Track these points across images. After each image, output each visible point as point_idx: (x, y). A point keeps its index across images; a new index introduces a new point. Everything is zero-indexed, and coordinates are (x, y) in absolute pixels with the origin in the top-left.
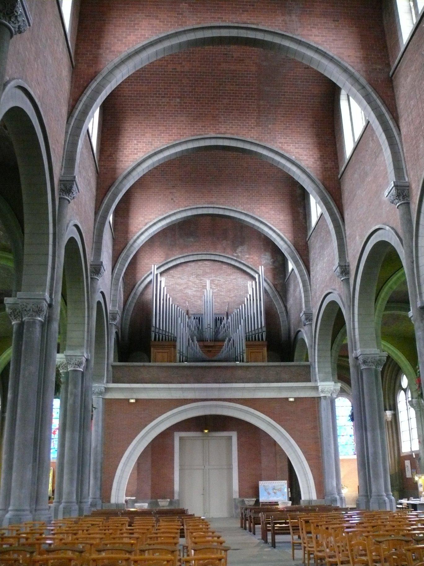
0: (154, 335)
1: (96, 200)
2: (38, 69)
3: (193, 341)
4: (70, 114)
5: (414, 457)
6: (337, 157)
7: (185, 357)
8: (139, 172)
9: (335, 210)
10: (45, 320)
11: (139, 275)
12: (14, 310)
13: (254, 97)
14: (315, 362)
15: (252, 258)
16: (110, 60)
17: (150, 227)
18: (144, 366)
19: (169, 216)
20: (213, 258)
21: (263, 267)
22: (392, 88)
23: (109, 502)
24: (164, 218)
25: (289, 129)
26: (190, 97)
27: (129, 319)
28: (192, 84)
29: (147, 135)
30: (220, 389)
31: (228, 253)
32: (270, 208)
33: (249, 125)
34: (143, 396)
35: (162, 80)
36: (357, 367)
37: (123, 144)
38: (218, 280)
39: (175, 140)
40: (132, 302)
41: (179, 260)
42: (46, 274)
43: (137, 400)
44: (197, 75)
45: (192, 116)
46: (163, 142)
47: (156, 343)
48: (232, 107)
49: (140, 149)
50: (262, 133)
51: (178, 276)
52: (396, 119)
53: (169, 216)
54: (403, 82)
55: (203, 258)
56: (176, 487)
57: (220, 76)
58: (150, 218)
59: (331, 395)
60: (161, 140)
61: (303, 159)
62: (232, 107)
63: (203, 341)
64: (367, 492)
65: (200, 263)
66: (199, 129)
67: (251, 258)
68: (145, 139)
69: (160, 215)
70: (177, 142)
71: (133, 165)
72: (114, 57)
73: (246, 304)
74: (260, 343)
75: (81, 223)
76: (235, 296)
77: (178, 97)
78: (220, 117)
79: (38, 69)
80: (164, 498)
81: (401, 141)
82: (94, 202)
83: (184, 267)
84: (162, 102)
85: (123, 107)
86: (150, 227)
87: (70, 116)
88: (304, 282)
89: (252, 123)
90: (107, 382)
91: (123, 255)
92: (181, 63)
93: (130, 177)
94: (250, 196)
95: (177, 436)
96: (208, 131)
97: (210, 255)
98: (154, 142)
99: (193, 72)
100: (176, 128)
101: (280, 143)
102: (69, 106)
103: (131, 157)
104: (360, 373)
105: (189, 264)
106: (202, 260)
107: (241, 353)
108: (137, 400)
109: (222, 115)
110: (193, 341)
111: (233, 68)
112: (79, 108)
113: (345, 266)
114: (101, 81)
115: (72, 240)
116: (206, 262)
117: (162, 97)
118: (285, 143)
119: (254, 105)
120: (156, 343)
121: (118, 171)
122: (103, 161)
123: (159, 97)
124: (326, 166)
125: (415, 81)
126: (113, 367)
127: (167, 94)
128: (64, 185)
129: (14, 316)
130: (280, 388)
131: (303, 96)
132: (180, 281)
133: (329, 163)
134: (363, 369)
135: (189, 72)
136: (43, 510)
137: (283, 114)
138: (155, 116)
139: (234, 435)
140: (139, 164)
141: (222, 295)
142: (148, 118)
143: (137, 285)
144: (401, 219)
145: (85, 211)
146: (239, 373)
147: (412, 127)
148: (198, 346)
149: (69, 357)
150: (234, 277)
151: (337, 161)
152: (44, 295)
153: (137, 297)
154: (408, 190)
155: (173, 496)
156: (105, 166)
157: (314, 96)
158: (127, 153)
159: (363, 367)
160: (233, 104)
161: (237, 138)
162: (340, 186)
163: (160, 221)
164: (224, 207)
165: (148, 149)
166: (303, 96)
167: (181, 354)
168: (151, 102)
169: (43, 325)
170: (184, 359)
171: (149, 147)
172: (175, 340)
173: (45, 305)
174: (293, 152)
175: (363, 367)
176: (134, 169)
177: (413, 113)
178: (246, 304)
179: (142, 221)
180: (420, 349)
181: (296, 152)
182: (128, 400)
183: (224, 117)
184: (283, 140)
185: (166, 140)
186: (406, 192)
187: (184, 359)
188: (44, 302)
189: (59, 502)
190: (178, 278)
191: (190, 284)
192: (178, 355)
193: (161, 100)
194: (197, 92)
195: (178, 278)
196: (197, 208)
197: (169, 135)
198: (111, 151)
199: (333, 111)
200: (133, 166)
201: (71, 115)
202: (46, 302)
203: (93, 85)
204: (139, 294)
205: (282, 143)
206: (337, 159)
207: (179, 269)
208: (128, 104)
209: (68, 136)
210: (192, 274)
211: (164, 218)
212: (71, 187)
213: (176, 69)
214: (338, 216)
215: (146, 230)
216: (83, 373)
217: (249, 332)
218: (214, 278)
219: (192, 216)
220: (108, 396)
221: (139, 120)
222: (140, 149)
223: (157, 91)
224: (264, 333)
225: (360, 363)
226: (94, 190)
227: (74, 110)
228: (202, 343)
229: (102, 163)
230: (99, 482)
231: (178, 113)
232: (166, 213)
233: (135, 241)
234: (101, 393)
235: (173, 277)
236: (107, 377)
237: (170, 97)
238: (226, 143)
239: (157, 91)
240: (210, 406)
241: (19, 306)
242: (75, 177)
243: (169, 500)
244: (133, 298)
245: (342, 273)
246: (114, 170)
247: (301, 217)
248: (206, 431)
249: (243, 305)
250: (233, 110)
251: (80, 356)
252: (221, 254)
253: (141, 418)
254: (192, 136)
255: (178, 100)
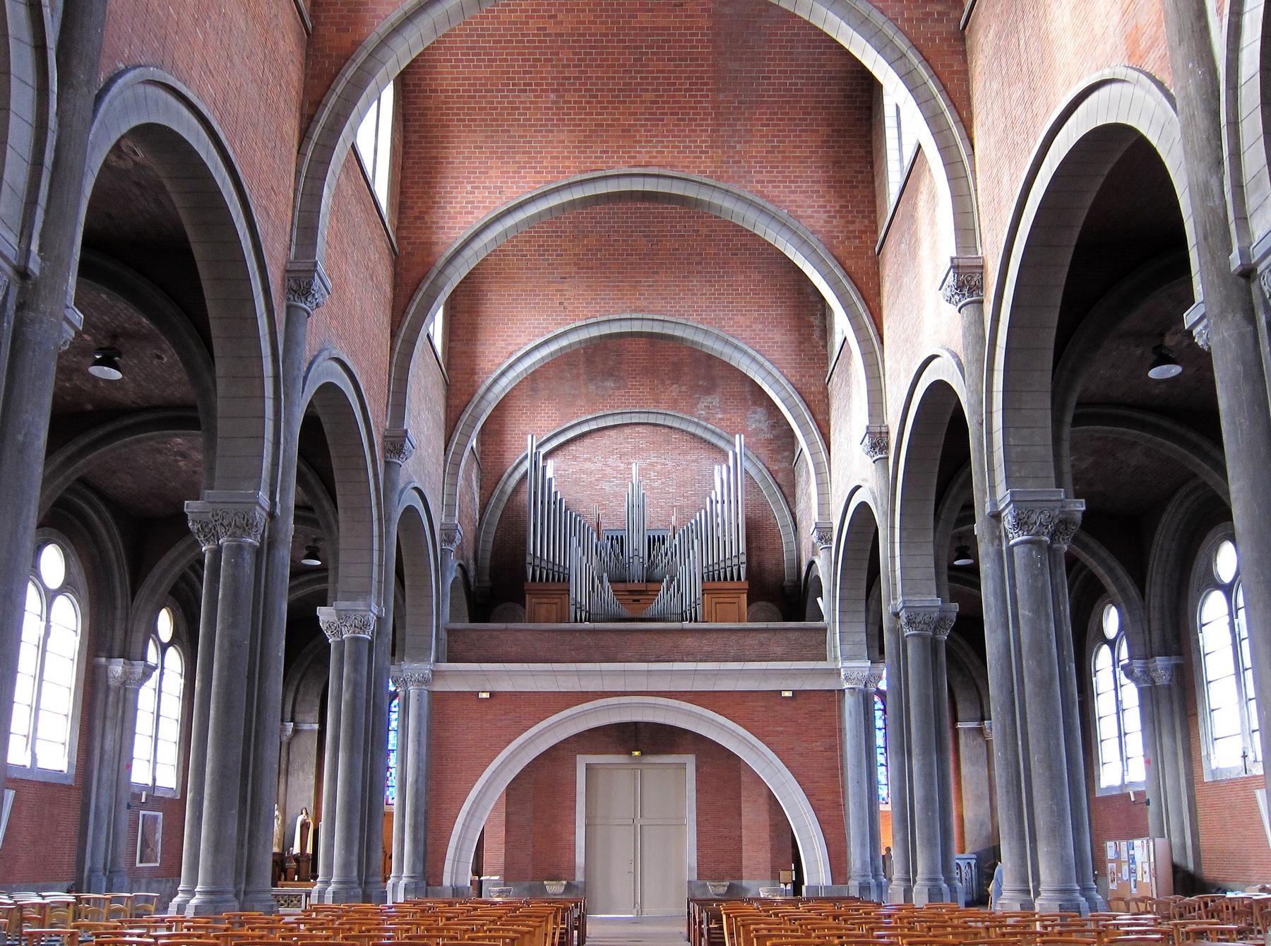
0: (531, 569)
1: (393, 309)
2: (205, 45)
3: (601, 582)
4: (304, 135)
5: (1133, 799)
6: (875, 207)
7: (586, 612)
8: (476, 249)
9: (866, 319)
10: (262, 543)
11: (508, 456)
12: (204, 525)
13: (706, 84)
14: (834, 622)
15: (730, 419)
16: (383, 16)
17: (519, 359)
18: (506, 630)
19: (556, 337)
20: (652, 419)
21: (742, 436)
22: (964, 53)
23: (441, 884)
24: (546, 343)
25: (778, 152)
26: (575, 90)
27: (491, 540)
28: (579, 60)
29: (492, 173)
30: (649, 673)
31: (681, 410)
32: (755, 318)
33: (695, 147)
34: (505, 686)
35: (519, 54)
36: (897, 632)
37: (445, 193)
38: (663, 464)
39: (548, 182)
40: (496, 507)
41: (578, 427)
42: (261, 456)
43: (492, 694)
44: (590, 41)
45: (580, 131)
46: (523, 187)
47: (537, 585)
48: (664, 108)
49: (479, 202)
50: (722, 162)
51: (585, 456)
52: (967, 126)
53: (556, 337)
54: (982, 40)
55: (634, 421)
56: (580, 859)
57: (635, 41)
58: (518, 342)
59: (865, 686)
60: (519, 182)
61: (804, 214)
62: (664, 108)
63: (625, 581)
64: (907, 872)
65: (627, 431)
66: (596, 157)
67: (727, 420)
68: (487, 181)
69: (537, 336)
70: (552, 186)
71: (465, 234)
72: (391, 8)
73: (708, 509)
74: (735, 585)
75: (353, 354)
76: (694, 495)
77: (553, 91)
78: (639, 131)
79: (205, 45)
80: (555, 878)
81: (974, 171)
82: (389, 313)
83: (596, 437)
84: (521, 102)
85: (442, 115)
86: (519, 359)
87: (304, 136)
88: (817, 465)
89: (702, 142)
90: (437, 661)
91: (465, 417)
92: (555, 16)
93: (459, 261)
94: (714, 294)
95: (582, 761)
96: (613, 162)
97: (611, 418)
98: (507, 187)
99: (579, 35)
100: (549, 156)
101: (758, 182)
102: (302, 115)
103: (461, 220)
104: (901, 643)
105: (607, 433)
106: (631, 424)
107: (693, 605)
108: (492, 694)
109: (641, 126)
110: (601, 582)
111: (661, 22)
112: (322, 121)
113: (881, 433)
114: (364, 62)
115: (330, 390)
116: (639, 429)
117: (520, 91)
118: (768, 182)
119: (706, 102)
120: (537, 585)
121: (436, 249)
122: (405, 228)
123: (514, 91)
124: (851, 228)
125: (1000, 38)
126: (450, 632)
127: (530, 85)
128: (295, 281)
129: (204, 537)
130: (765, 673)
131: (807, 78)
132: (588, 465)
133: (857, 220)
134: (907, 636)
135: (572, 35)
136: (259, 892)
137: (767, 119)
138: (508, 131)
139: (690, 761)
140: (476, 235)
141: (669, 493)
142: (493, 137)
143: (506, 475)
144: (964, 336)
145: (363, 330)
146: (690, 642)
147: (992, 139)
148: (611, 591)
149: (343, 613)
150: (694, 458)
151: (875, 217)
152: (255, 495)
153: (505, 498)
154: (982, 273)
155: (574, 875)
156: (410, 238)
157: (830, 78)
158: (452, 211)
159: (908, 632)
160: (663, 102)
161: (670, 173)
162: (878, 268)
163: (537, 348)
164: (662, 318)
165: (494, 203)
166: (807, 78)
167: (578, 606)
168: (498, 103)
169: (258, 552)
170: (583, 617)
171: (496, 198)
172: (566, 580)
173: (260, 516)
174: (784, 201)
175: (908, 632)
176: (466, 244)
177: (995, 108)
178: (708, 509)
179: (502, 348)
180: (986, 597)
181: (791, 201)
182: (478, 693)
183: (646, 131)
184: (765, 176)
185: (529, 182)
186: (975, 279)
187: (583, 617)
188: (257, 507)
189: (327, 883)
190: (586, 460)
191: (609, 471)
192: (572, 609)
193: (519, 97)
194: (591, 78)
195: (586, 460)
196: (609, 321)
197: (535, 173)
198: (420, 207)
199: (870, 109)
200: (465, 237)
201: (307, 135)
202: (263, 508)
203: (350, 72)
204: (509, 490)
205: (763, 182)
206: (874, 212)
207: (588, 442)
208: (452, 109)
209: (303, 180)
210: (612, 453)
211: (546, 343)
212: (402, 446)
213: (545, 29)
214: (872, 331)
215: (511, 366)
216: (371, 642)
217: (707, 567)
218: (655, 460)
219: (601, 337)
220: (438, 687)
221: (476, 142)
222: (479, 202)
223: (508, 79)
224: (741, 566)
225: (903, 624)
226: (388, 289)
227: (312, 125)
228: (621, 586)
229: (405, 231)
230: (421, 848)
231: (553, 125)
232: (548, 332)
233: (489, 389)
234: (425, 681)
235: (575, 458)
236: (437, 652)
237: (536, 91)
238: (650, 186)
239: (508, 79)
240: (621, 706)
241: (210, 515)
242: (315, 264)
243: (564, 882)
244: (499, 499)
245: (873, 446)
246: (428, 247)
247: (816, 335)
248: (637, 753)
249: (703, 511)
250: (666, 114)
251: (364, 610)
252: (668, 412)
253: (500, 727)
254: (582, 172)
255: (553, 96)
